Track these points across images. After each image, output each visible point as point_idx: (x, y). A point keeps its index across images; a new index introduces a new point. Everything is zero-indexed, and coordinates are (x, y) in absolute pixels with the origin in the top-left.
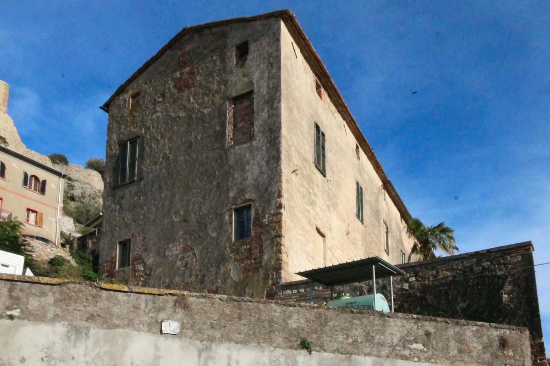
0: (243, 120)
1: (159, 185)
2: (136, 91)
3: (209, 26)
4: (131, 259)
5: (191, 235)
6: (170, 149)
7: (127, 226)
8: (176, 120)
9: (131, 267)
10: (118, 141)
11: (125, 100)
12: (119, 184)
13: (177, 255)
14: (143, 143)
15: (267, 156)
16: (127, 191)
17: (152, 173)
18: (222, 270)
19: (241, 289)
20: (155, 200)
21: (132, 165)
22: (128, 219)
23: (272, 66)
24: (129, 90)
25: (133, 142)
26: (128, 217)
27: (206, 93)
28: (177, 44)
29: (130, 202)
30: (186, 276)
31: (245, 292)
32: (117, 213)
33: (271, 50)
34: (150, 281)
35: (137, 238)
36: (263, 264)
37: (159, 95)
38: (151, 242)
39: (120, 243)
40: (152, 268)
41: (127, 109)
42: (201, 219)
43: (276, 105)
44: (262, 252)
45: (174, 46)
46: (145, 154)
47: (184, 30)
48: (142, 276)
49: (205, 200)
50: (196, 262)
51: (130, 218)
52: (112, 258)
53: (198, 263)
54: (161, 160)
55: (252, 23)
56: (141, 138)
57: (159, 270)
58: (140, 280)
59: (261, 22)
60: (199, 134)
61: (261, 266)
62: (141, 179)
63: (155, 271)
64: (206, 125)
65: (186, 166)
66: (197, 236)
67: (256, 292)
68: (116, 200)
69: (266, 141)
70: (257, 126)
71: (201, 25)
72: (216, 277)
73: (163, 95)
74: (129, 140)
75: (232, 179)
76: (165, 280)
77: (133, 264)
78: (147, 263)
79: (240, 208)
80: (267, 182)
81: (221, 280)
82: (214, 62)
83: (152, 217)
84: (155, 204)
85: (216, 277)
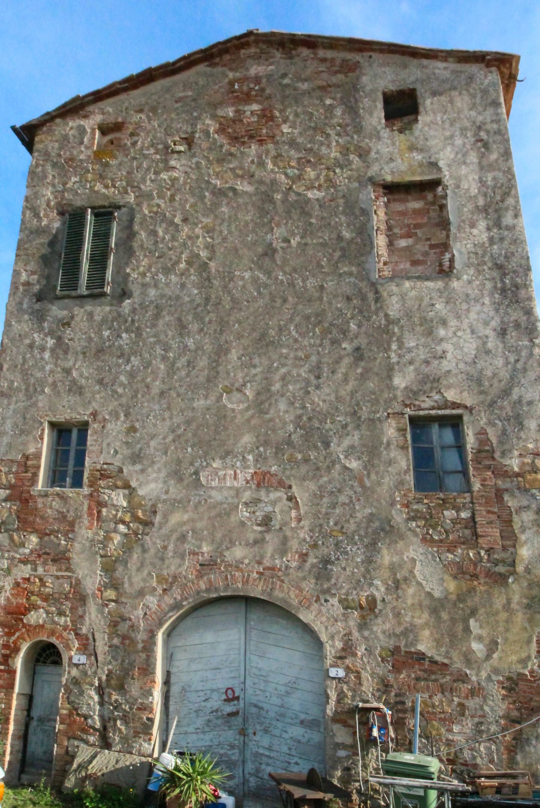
0: (408, 235)
1: (179, 320)
2: (111, 119)
3: (311, 42)
4: (86, 475)
5: (279, 450)
6: (211, 248)
7: (76, 389)
8: (226, 196)
9: (86, 490)
10: (58, 204)
11: (82, 131)
12: (58, 292)
13: (238, 492)
14: (131, 221)
15: (498, 319)
16: (79, 312)
17: (156, 286)
18: (386, 557)
19: (453, 621)
20: (167, 348)
21: (99, 261)
22: (81, 375)
23: (486, 145)
24: (93, 113)
25: (104, 215)
26: (83, 371)
27: (309, 161)
28: (227, 57)
29: (90, 340)
30: (269, 549)
31: (467, 630)
32: (47, 355)
33: (480, 118)
34: (147, 538)
35: (109, 426)
36: (520, 568)
37: (177, 138)
38: (153, 443)
39: (52, 425)
40: (154, 505)
41: (87, 148)
42: (310, 419)
43: (508, 219)
44: (510, 538)
45: (217, 60)
46: (135, 245)
47: (250, 33)
48: (123, 522)
49: (318, 377)
50: (299, 520)
51: (86, 374)
52: (27, 458)
53: (306, 523)
54: (183, 265)
55: (425, 62)
56: (124, 210)
57: (175, 518)
58: (115, 531)
59: (445, 65)
60: (293, 234)
61: (514, 573)
62: (125, 294)
63: (165, 517)
64: (313, 221)
65: (259, 293)
66: (299, 456)
67: (506, 640)
68: (46, 325)
69: (489, 285)
70: (461, 253)
71: (294, 35)
72: (368, 571)
73: (189, 141)
74: (93, 208)
75: (400, 348)
76: (200, 547)
77: (91, 485)
78: (141, 492)
79: (419, 418)
80: (504, 374)
81: (385, 582)
82: (330, 109)
83: (157, 386)
84: (164, 358)
85: (368, 571)
